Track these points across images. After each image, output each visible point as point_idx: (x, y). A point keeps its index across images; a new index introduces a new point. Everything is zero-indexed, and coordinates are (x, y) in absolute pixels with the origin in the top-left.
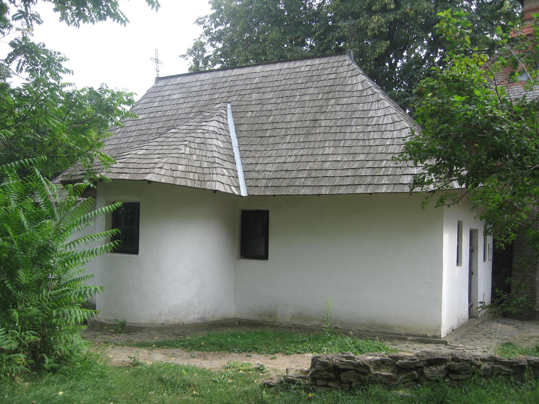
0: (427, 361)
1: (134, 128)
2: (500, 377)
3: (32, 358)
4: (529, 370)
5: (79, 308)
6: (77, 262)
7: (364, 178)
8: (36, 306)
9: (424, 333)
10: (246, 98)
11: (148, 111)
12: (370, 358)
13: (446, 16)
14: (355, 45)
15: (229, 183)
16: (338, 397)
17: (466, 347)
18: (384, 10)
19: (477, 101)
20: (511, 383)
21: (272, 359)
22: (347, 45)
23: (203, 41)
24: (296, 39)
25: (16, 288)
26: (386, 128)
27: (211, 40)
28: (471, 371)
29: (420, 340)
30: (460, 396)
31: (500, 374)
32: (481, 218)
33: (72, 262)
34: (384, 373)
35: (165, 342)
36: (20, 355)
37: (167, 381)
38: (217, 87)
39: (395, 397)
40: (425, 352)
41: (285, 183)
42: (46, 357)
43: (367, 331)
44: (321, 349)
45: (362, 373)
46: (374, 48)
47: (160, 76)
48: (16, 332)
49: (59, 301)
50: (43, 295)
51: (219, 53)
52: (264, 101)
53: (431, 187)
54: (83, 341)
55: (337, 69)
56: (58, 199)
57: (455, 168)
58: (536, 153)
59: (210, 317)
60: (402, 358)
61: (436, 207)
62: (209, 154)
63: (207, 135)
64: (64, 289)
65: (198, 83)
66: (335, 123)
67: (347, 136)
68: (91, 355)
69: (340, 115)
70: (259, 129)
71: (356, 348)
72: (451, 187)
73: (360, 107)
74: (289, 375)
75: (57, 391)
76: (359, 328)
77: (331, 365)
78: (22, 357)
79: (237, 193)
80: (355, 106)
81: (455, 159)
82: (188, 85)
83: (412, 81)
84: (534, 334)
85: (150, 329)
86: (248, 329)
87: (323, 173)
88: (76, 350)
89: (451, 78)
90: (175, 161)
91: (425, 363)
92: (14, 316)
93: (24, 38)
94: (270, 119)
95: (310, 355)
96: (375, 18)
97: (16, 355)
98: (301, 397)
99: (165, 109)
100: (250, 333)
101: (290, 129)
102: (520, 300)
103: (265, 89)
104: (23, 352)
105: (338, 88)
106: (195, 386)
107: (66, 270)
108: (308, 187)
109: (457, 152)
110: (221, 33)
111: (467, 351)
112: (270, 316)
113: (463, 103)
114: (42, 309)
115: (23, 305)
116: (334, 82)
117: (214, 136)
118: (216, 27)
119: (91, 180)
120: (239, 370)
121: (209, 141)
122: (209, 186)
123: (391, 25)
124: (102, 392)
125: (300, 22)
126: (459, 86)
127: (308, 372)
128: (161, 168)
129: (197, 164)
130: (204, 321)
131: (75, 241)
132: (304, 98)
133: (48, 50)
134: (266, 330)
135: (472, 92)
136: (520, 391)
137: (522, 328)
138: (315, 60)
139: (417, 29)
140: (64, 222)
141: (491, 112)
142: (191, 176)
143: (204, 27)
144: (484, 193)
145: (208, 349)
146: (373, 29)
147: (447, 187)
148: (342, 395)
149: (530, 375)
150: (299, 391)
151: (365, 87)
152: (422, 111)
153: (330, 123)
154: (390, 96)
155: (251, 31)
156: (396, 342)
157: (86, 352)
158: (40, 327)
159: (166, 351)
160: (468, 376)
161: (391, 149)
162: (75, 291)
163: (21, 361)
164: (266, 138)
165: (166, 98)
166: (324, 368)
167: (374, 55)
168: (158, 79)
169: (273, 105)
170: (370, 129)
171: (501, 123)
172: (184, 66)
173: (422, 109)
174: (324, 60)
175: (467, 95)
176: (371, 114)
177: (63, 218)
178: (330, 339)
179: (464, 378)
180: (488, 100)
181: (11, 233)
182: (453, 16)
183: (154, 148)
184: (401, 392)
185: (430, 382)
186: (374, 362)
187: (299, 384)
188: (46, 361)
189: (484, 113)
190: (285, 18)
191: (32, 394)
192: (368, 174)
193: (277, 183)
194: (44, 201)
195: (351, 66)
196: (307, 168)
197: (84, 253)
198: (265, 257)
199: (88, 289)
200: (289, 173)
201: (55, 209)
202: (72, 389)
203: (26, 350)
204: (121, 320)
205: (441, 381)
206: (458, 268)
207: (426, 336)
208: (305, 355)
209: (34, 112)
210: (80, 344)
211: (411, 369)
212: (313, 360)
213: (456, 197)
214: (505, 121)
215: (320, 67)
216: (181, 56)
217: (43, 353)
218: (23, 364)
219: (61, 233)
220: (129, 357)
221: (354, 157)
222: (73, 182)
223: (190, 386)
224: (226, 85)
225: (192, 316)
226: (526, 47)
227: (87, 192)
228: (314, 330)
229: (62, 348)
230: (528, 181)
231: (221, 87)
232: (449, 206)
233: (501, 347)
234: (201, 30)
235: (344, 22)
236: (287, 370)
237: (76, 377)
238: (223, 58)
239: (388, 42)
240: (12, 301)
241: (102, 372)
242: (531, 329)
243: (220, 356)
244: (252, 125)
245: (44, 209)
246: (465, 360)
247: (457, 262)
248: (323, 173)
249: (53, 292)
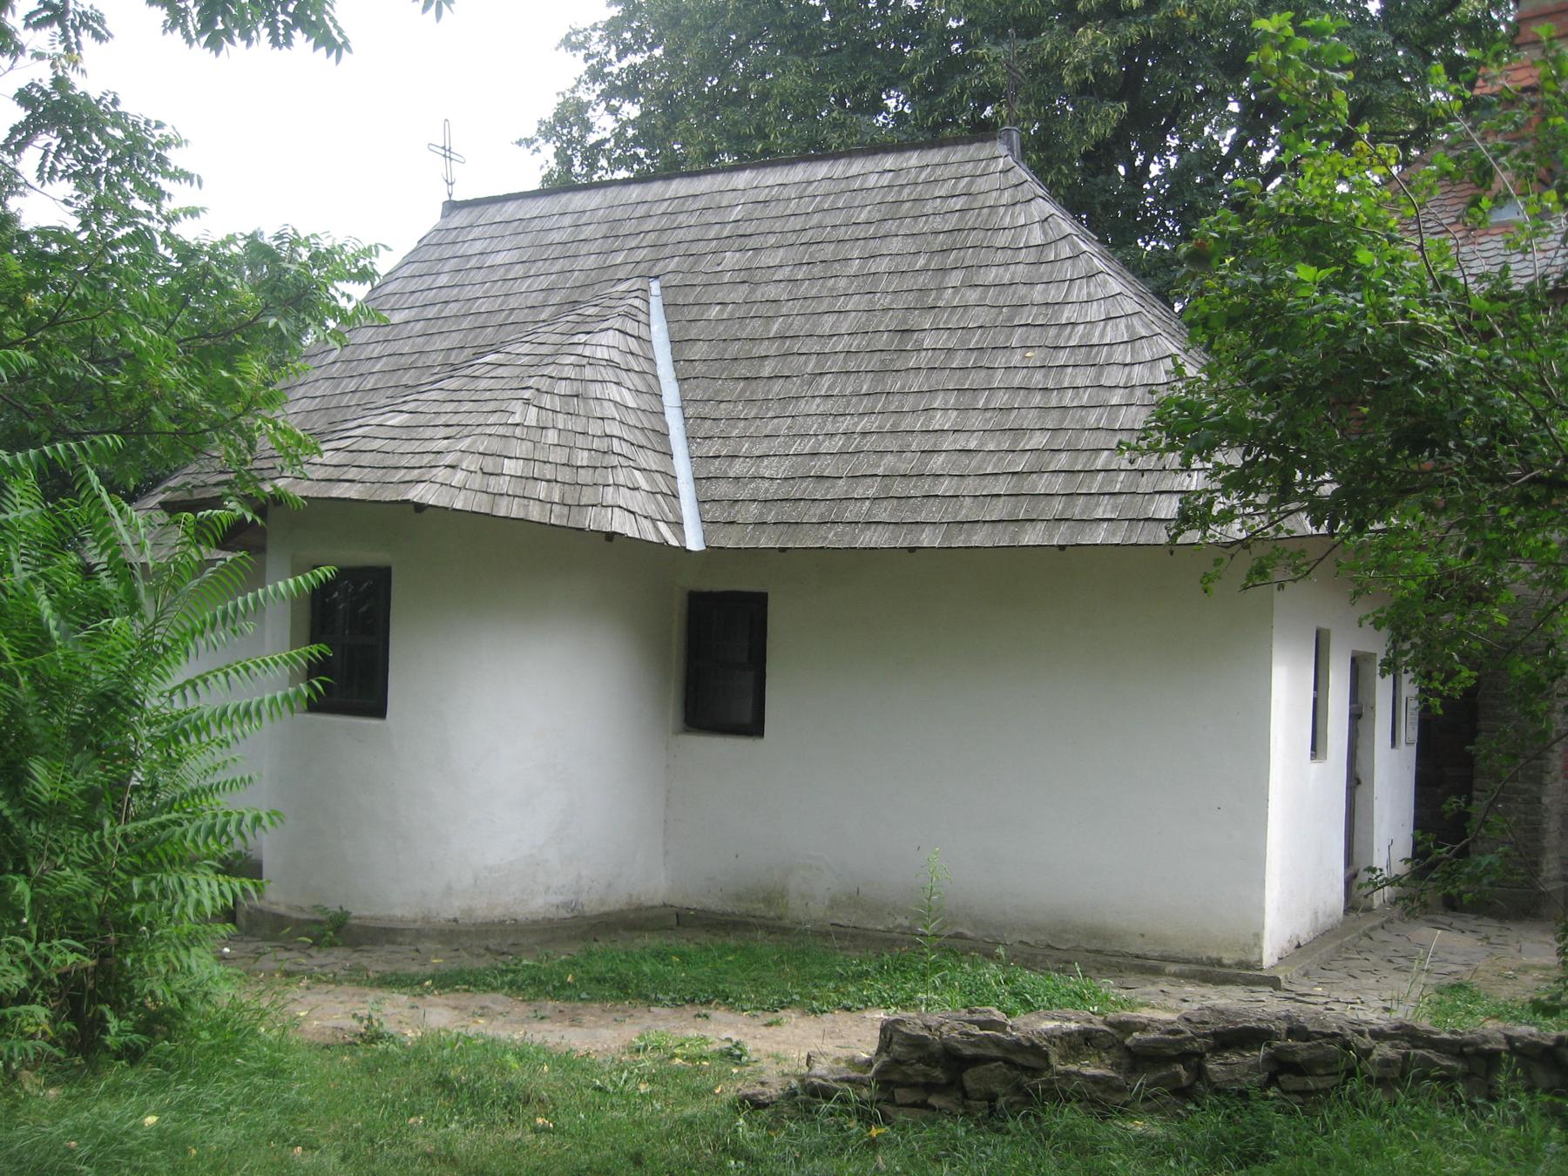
0: (1215, 1035)
1: (378, 350)
2: (1426, 1083)
3: (68, 1018)
4: (1510, 1064)
5: (211, 873)
6: (204, 738)
7: (1043, 502)
8: (84, 867)
9: (1214, 955)
11: (421, 299)
12: (1049, 1025)
13: (1280, 29)
14: (1027, 111)
16: (954, 1137)
17: (1335, 995)
18: (1112, 12)
19: (1362, 283)
20: (1458, 1101)
21: (769, 1025)
22: (1004, 113)
23: (585, 98)
24: (855, 92)
25: (26, 813)
26: (1110, 355)
27: (606, 95)
28: (1342, 1066)
30: (1309, 1138)
31: (1425, 1076)
32: (1377, 625)
33: (188, 740)
34: (1090, 1071)
35: (461, 971)
36: (35, 1008)
37: (461, 1089)
38: (622, 232)
39: (1120, 1138)
40: (1212, 1009)
41: (815, 513)
42: (109, 1015)
44: (911, 999)
45: (1025, 1069)
46: (1081, 124)
47: (457, 197)
48: (22, 942)
49: (150, 855)
50: (102, 836)
51: (630, 132)
53: (1236, 531)
54: (218, 970)
55: (971, 184)
56: (148, 557)
57: (1299, 476)
58: (1536, 436)
59: (593, 902)
60: (1144, 1028)
61: (1245, 588)
62: (595, 428)
63: (588, 373)
64: (164, 817)
65: (567, 220)
67: (998, 379)
68: (241, 1007)
69: (978, 317)
70: (741, 355)
71: (1014, 994)
72: (1288, 531)
73: (1037, 294)
74: (813, 1072)
75: (141, 1113)
76: (1025, 939)
77: (937, 1047)
78: (39, 1014)
79: (674, 542)
80: (1022, 290)
81: (1299, 451)
82: (536, 225)
83: (1189, 216)
84: (1535, 960)
85: (420, 934)
86: (703, 938)
87: (926, 486)
88: (200, 994)
89: (1291, 212)
90: (495, 445)
91: (1210, 1041)
92: (18, 896)
93: (60, 83)
94: (775, 328)
95: (881, 1015)
96: (1086, 35)
97: (22, 1008)
98: (849, 1137)
99: (471, 295)
100: (707, 950)
101: (833, 357)
102: (1484, 863)
103: (762, 238)
104: (44, 999)
105: (973, 239)
106: (541, 1101)
107: (171, 764)
108: (880, 527)
109: (1302, 430)
110: (636, 73)
111: (1336, 1006)
112: (768, 900)
113: (1324, 288)
114: (101, 877)
115: (44, 865)
116: (960, 219)
117: (608, 374)
118: (621, 55)
119: (247, 500)
120: (673, 1056)
121: (596, 390)
122: (593, 520)
123: (1127, 53)
124: (273, 1118)
125: (867, 44)
126: (1316, 236)
127: (869, 1063)
129: (559, 456)
131: (188, 682)
132: (873, 266)
133: (126, 114)
134: (756, 940)
135: (1350, 252)
136: (1483, 1125)
137: (1500, 940)
138: (907, 155)
139: (1207, 70)
140: (167, 622)
141: (1404, 313)
142: (541, 490)
143: (588, 57)
144: (1386, 549)
145: (584, 995)
146: (1079, 68)
147: (1278, 530)
148: (967, 1132)
149: (1514, 1078)
150: (842, 1119)
151: (1052, 236)
152: (1206, 309)
153: (948, 339)
154: (1125, 263)
155: (724, 71)
156: (1131, 979)
157: (226, 1000)
158: (94, 927)
159: (463, 999)
160: (1332, 1081)
161: (1125, 418)
162: (198, 823)
163: (38, 1024)
164: (762, 383)
165: (473, 262)
166: (916, 1055)
167: (1080, 142)
168: (452, 207)
169: (782, 285)
170: (1062, 357)
171: (1436, 349)
172: (529, 169)
173: (1208, 303)
174: (935, 156)
175: (1338, 262)
176: (1067, 314)
177: (162, 612)
178: (937, 967)
179: (1321, 1086)
180: (1395, 281)
181: (9, 654)
182: (1301, 32)
183: (435, 408)
184: (1138, 1126)
185: (1222, 1098)
186: (1061, 1039)
187: (844, 1100)
188: (110, 1026)
189: (1382, 316)
190: (823, 33)
191: (66, 1121)
192: (1056, 489)
193: (790, 513)
194: (108, 563)
195: (1010, 174)
196: (880, 471)
197: (225, 712)
198: (755, 728)
199: (235, 817)
200: (828, 484)
201: (141, 586)
202: (184, 1107)
203: (52, 995)
204: (333, 907)
205: (1255, 1093)
206: (1315, 767)
207: (1220, 963)
208: (867, 1014)
209: (82, 303)
210: (209, 976)
211: (1170, 1060)
212: (883, 1030)
213: (1303, 561)
214: (1445, 339)
215: (923, 176)
216: (519, 143)
217: (102, 1001)
218: (44, 1033)
219: (158, 656)
220: (354, 1016)
221: (1015, 441)
222: (194, 506)
223: (527, 1102)
224: (649, 225)
225: (539, 899)
226: (1515, 123)
227: (234, 536)
229: (157, 990)
230: (1511, 516)
231: (632, 230)
232: (1281, 586)
233: (1436, 997)
235: (996, 44)
236: (809, 1057)
237: (198, 1073)
238: (642, 146)
239: (1124, 107)
240: (12, 851)
241: (273, 1059)
242: (1526, 945)
243: (618, 1016)
244: (722, 345)
245: (107, 583)
246: (1324, 1035)
247: (1314, 748)
248: (926, 486)
249: (133, 825)
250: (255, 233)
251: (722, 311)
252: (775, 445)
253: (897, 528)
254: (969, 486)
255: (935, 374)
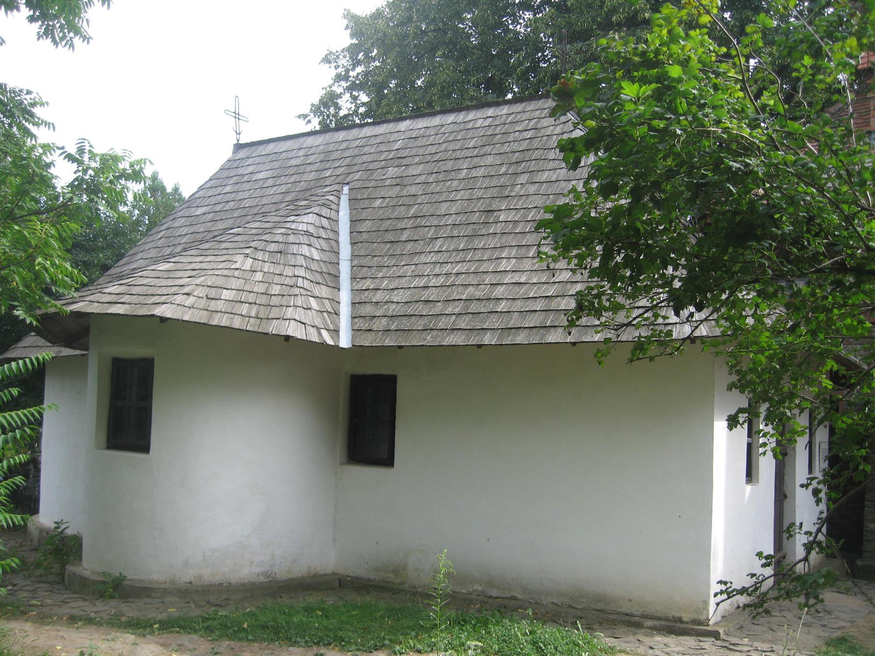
1: (185, 230)
9: (677, 614)
10: (376, 175)
11: (214, 200)
15: (316, 324)
27: (352, 88)
29: (668, 627)
38: (332, 158)
41: (420, 324)
43: (570, 606)
47: (242, 142)
52: (407, 179)
59: (282, 572)
65: (302, 153)
66: (523, 216)
76: (555, 601)
79: (330, 342)
82: (284, 155)
85: (166, 592)
87: (491, 306)
90: (220, 282)
94: (412, 211)
99: (242, 197)
101: (445, 228)
105: (536, 154)
108: (460, 332)
112: (396, 572)
117: (305, 239)
121: (294, 249)
122: (273, 328)
128: (188, 294)
129: (261, 288)
130: (271, 579)
132: (474, 173)
142: (244, 309)
145: (250, 637)
153: (515, 215)
156: (621, 630)
165: (246, 178)
168: (239, 147)
169: (420, 186)
193: (406, 324)
196: (464, 297)
198: (388, 462)
206: (749, 488)
207: (680, 620)
215: (509, 119)
216: (299, 117)
228: (472, 600)
234: (330, 72)
244: (380, 222)
248: (491, 306)
250: (154, 173)
251: (382, 202)
252: (404, 282)
253: (470, 332)
254: (518, 305)
255: (505, 237)
